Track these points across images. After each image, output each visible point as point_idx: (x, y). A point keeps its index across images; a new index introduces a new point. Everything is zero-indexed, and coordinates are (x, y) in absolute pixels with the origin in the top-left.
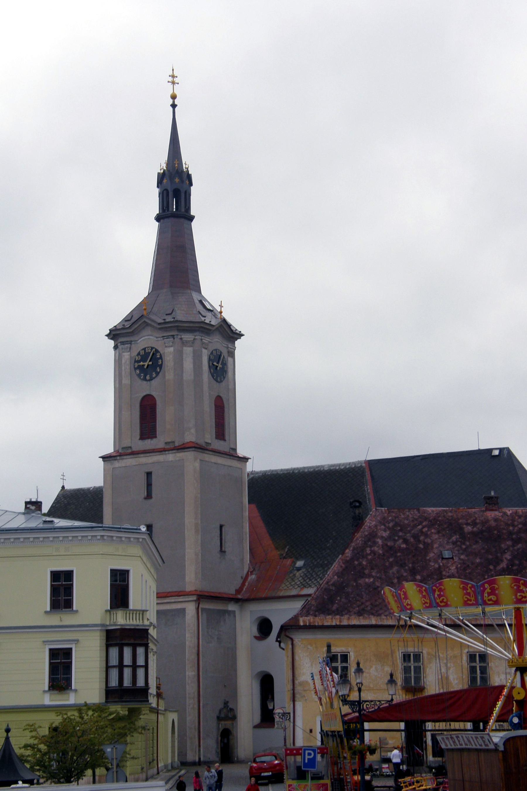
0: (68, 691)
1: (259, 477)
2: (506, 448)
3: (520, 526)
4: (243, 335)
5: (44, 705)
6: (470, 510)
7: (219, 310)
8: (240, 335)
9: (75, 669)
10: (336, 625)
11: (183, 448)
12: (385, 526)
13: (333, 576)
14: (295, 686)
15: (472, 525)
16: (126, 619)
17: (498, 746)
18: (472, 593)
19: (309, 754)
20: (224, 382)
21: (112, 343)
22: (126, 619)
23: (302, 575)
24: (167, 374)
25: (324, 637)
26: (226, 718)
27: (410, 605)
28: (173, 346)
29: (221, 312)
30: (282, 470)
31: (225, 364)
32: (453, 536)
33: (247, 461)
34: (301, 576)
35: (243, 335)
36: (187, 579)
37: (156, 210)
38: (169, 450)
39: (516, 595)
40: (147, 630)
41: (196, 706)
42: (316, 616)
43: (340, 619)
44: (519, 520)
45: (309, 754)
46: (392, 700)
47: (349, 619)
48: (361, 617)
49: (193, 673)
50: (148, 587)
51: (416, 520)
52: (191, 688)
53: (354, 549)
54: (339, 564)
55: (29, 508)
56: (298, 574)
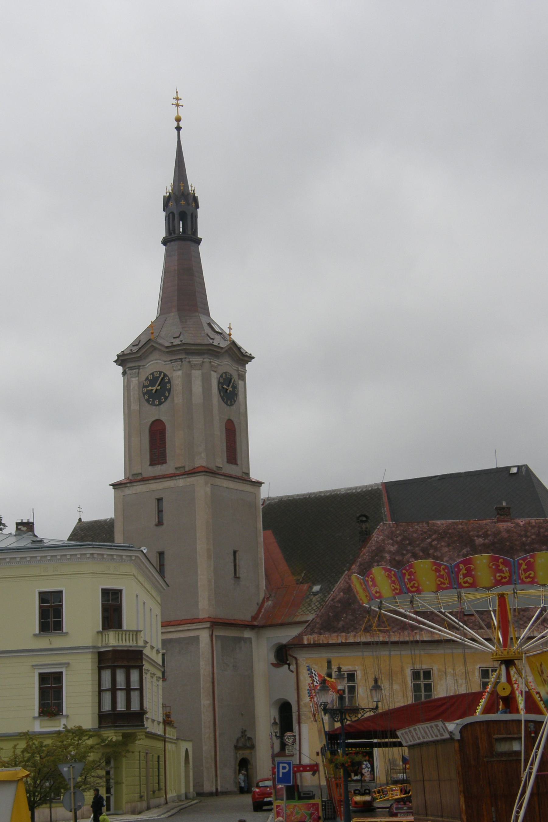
0: (58, 717)
2: (525, 465)
3: (533, 537)
4: (254, 358)
5: (35, 732)
6: (481, 522)
7: (228, 333)
8: (250, 358)
9: (66, 693)
10: (342, 643)
11: (193, 472)
12: (392, 540)
13: (339, 593)
14: (300, 707)
15: (483, 537)
16: (118, 640)
17: (454, 734)
18: (445, 575)
19: (284, 768)
20: (235, 405)
21: (120, 369)
22: (118, 640)
23: (318, 599)
25: (326, 655)
26: (245, 747)
27: (379, 592)
28: (185, 375)
29: (230, 335)
30: (298, 495)
31: (235, 387)
32: (464, 549)
34: (318, 601)
35: (254, 358)
36: (200, 606)
37: (162, 233)
39: (495, 576)
40: (141, 652)
41: (212, 735)
42: (320, 634)
43: (346, 636)
44: (533, 531)
45: (284, 768)
46: (377, 707)
47: (355, 636)
48: (368, 634)
49: (208, 702)
50: (147, 610)
51: (425, 533)
52: (206, 717)
53: (361, 564)
54: (345, 581)
55: (20, 529)
56: (314, 599)
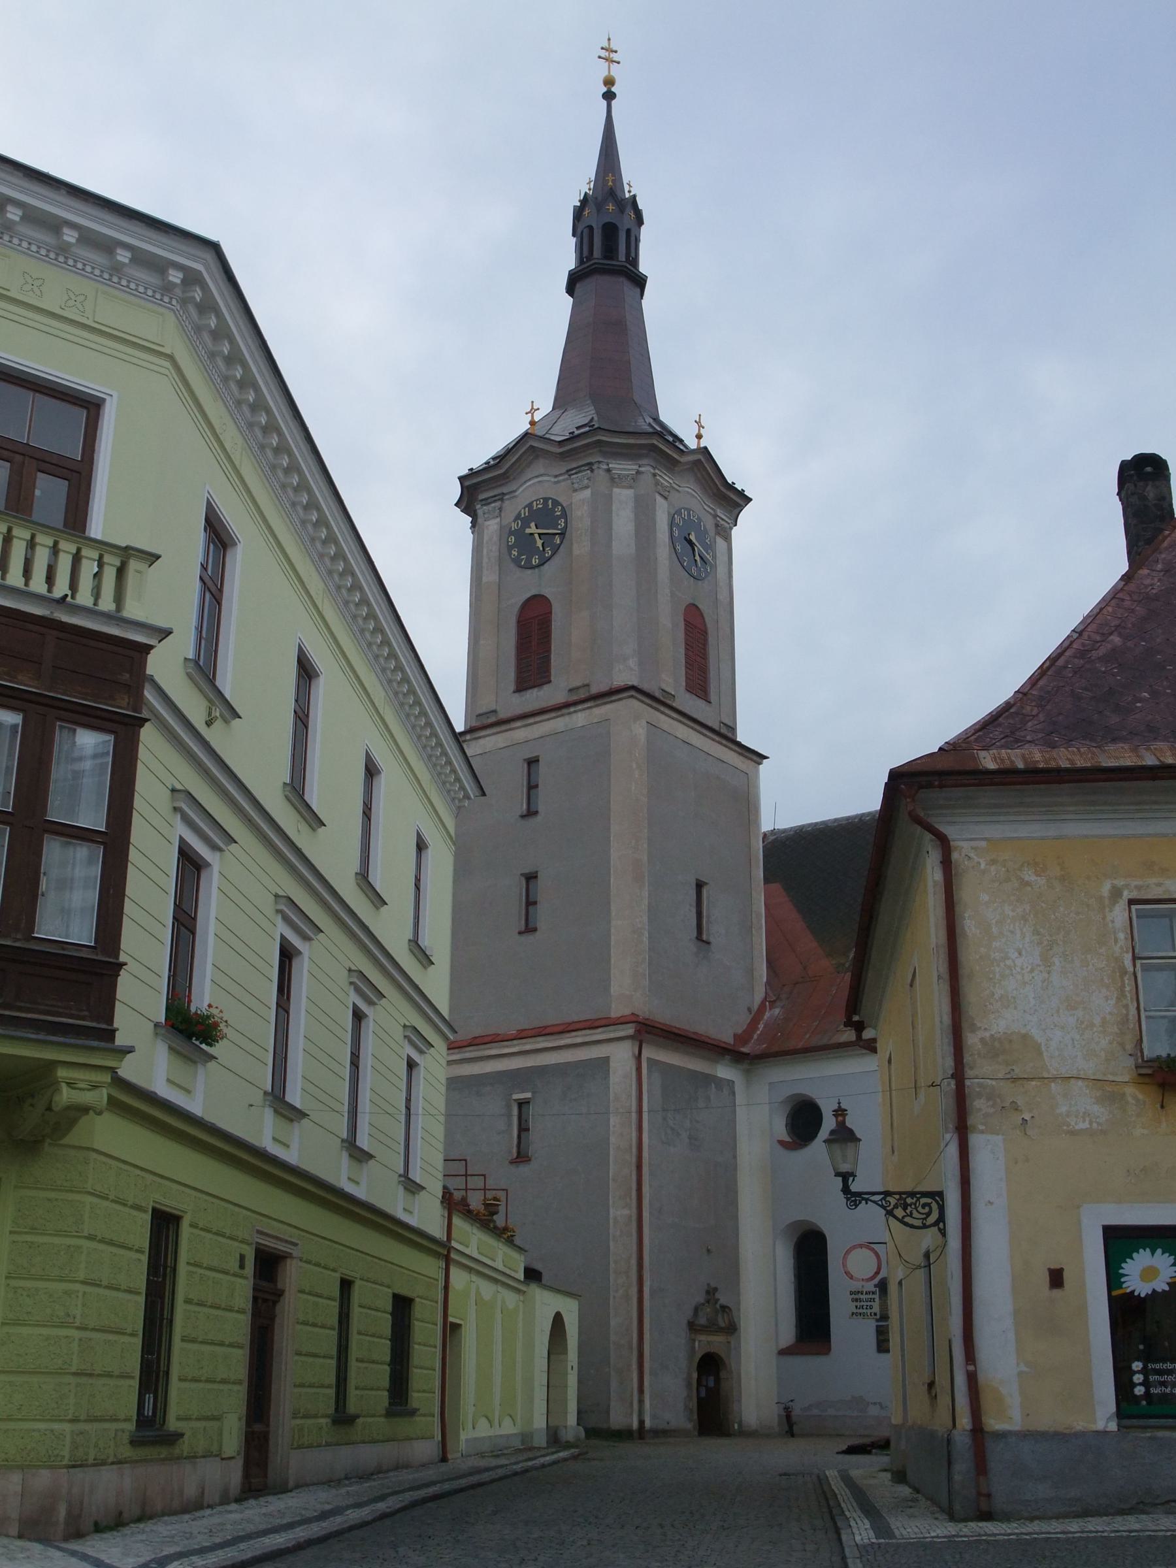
1: (788, 838)
14: (967, 1058)
24: (575, 546)
26: (711, 1328)
30: (836, 820)
33: (760, 763)
36: (614, 989)
38: (575, 703)
49: (626, 1212)
52: (621, 1248)
